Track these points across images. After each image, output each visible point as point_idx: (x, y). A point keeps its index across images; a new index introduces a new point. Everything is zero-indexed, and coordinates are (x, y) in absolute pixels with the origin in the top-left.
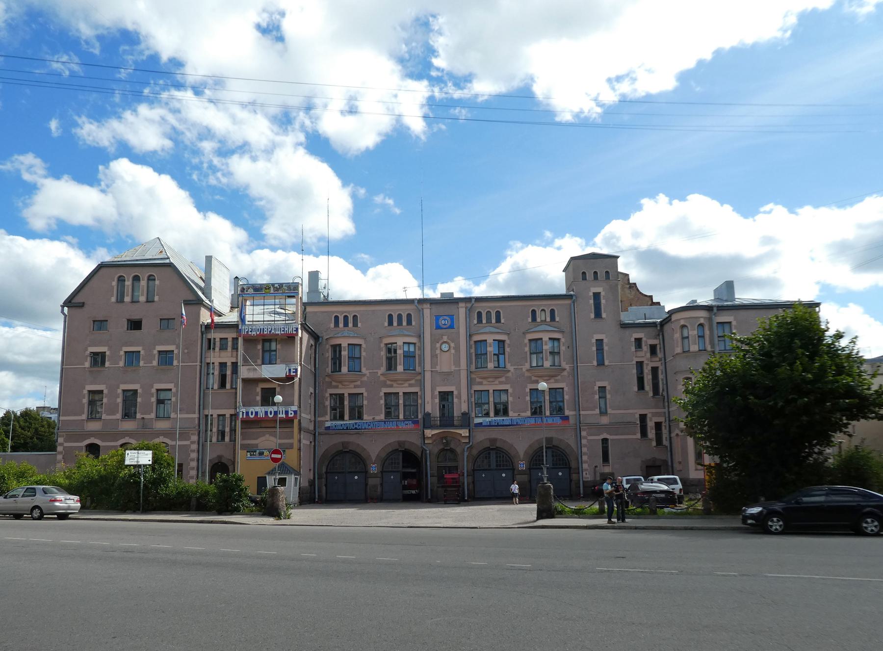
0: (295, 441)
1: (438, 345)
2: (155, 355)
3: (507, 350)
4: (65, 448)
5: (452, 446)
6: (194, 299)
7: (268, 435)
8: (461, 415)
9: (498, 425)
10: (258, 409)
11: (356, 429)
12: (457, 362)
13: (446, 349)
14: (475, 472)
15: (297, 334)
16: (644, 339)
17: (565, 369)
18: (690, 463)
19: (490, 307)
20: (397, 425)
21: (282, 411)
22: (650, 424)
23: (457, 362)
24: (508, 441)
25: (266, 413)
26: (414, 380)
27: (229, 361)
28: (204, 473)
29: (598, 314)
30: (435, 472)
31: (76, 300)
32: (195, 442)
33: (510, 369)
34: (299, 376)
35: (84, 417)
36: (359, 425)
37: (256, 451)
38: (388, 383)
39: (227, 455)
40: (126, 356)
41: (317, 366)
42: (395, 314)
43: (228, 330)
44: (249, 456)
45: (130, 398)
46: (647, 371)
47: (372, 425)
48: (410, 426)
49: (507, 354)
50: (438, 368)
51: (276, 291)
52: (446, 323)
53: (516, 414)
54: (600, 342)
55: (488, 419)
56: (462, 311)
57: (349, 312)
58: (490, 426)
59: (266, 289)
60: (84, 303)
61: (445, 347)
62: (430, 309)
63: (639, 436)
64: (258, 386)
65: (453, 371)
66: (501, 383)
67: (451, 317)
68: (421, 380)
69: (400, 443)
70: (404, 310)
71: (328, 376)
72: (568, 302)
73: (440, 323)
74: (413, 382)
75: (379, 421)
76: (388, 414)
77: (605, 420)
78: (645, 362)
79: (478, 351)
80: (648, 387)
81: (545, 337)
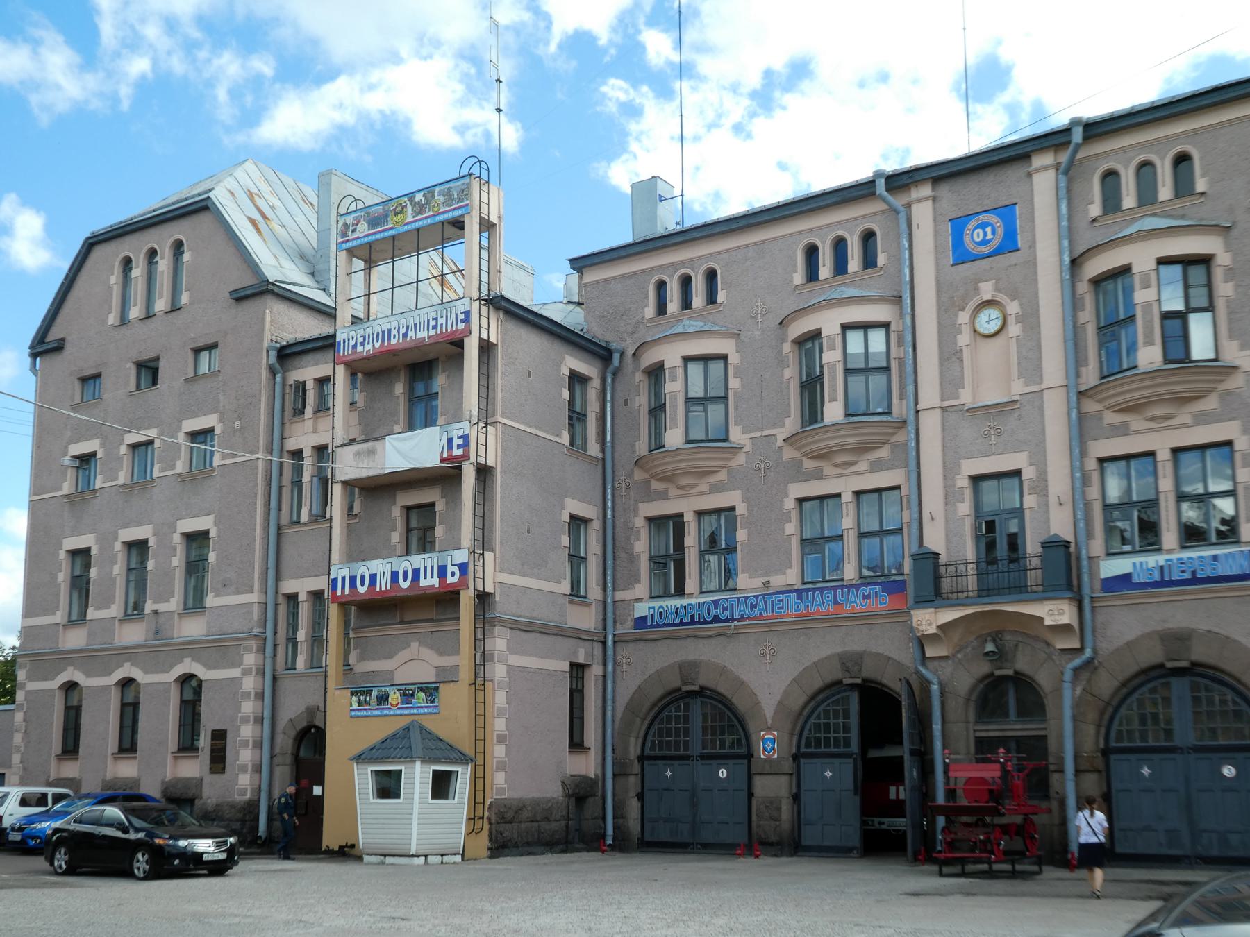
1: (963, 317)
3: (1224, 289)
5: (1022, 663)
6: (256, 282)
7: (417, 644)
8: (1040, 550)
9: (1194, 580)
11: (717, 619)
12: (1031, 366)
13: (993, 327)
14: (1113, 757)
17: (1236, 368)
20: (836, 602)
21: (432, 567)
23: (1031, 366)
24: (1238, 638)
26: (887, 447)
31: (54, 335)
33: (1237, 363)
35: (59, 617)
36: (725, 609)
37: (369, 693)
40: (133, 458)
41: (608, 438)
42: (823, 243)
44: (355, 706)
47: (761, 605)
48: (879, 600)
49: (1220, 304)
50: (966, 397)
51: (420, 213)
52: (990, 236)
55: (1153, 561)
57: (690, 262)
58: (1163, 583)
59: (396, 214)
61: (988, 321)
62: (934, 199)
64: (395, 504)
65: (1017, 398)
66: (1201, 419)
68: (906, 444)
69: (849, 661)
73: (967, 240)
74: (883, 453)
75: (782, 592)
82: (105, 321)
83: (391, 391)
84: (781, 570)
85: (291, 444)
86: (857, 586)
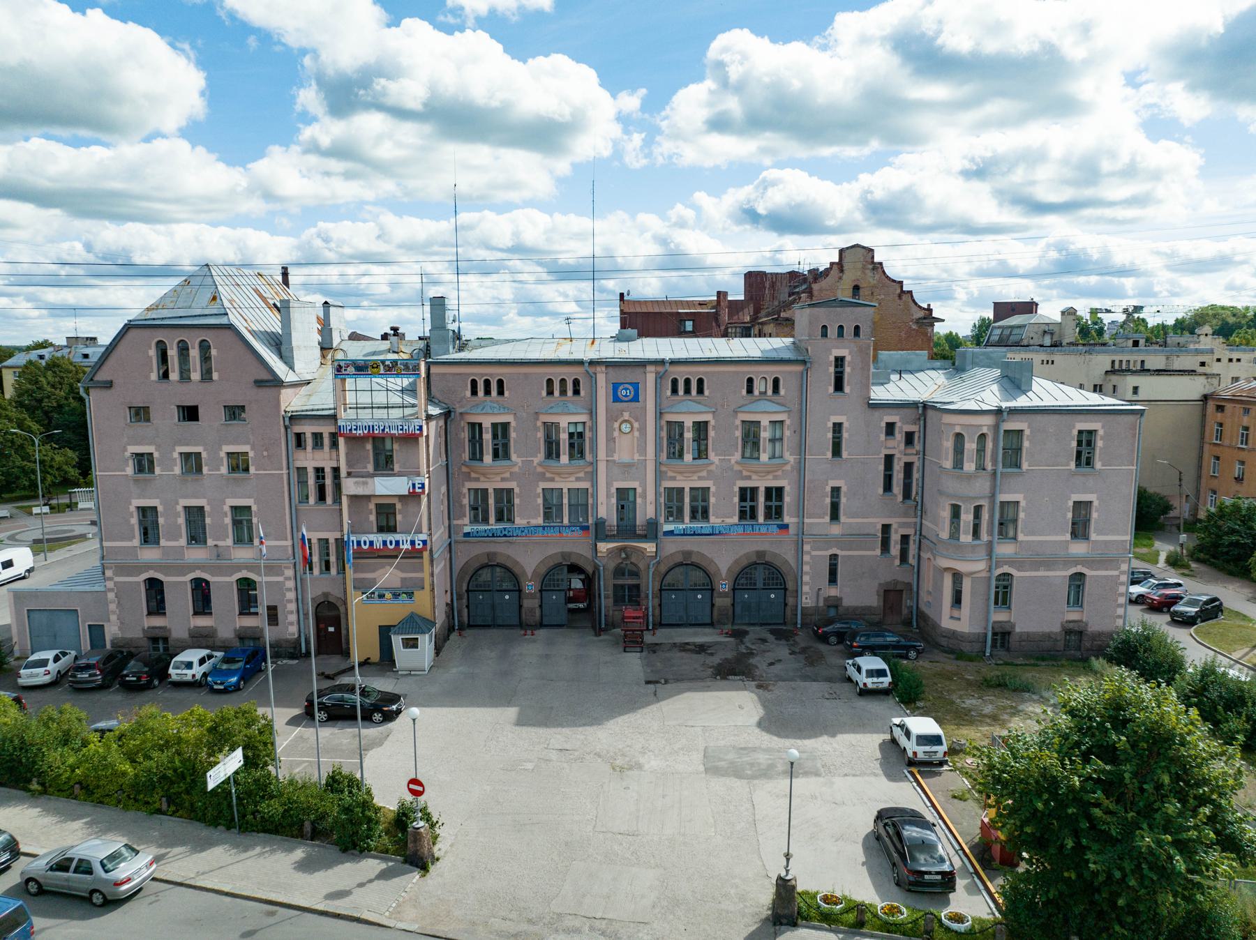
0: (426, 575)
1: (616, 425)
2: (222, 458)
4: (116, 583)
9: (694, 534)
10: (372, 537)
12: (642, 450)
15: (421, 435)
16: (898, 425)
18: (944, 607)
19: (690, 373)
22: (895, 538)
23: (642, 450)
25: (385, 543)
27: (332, 536)
28: (306, 615)
29: (839, 386)
30: (611, 592)
32: (290, 579)
34: (426, 492)
38: (548, 475)
39: (336, 592)
43: (321, 422)
45: (195, 516)
46: (898, 468)
50: (616, 457)
53: (719, 520)
54: (838, 427)
55: (681, 526)
56: (651, 378)
57: (491, 375)
58: (684, 535)
60: (112, 382)
61: (626, 428)
63: (878, 552)
66: (700, 478)
67: (636, 386)
70: (570, 374)
71: (464, 464)
72: (799, 368)
76: (547, 516)
77: (836, 530)
78: (896, 456)
79: (673, 438)
80: (897, 488)
81: (765, 421)
82: (148, 377)
83: (364, 448)
84: (535, 517)
85: (299, 464)
86: (569, 527)
